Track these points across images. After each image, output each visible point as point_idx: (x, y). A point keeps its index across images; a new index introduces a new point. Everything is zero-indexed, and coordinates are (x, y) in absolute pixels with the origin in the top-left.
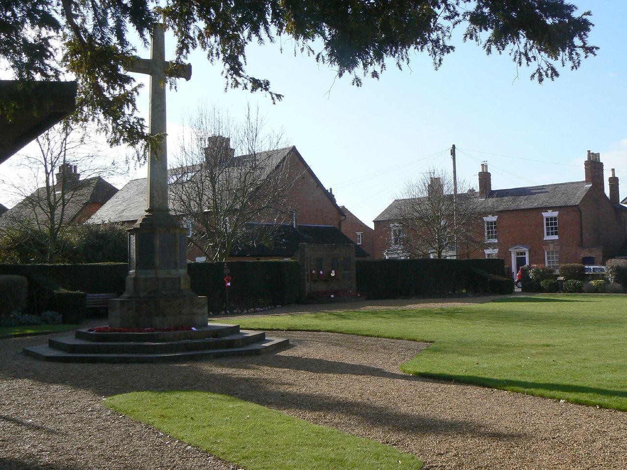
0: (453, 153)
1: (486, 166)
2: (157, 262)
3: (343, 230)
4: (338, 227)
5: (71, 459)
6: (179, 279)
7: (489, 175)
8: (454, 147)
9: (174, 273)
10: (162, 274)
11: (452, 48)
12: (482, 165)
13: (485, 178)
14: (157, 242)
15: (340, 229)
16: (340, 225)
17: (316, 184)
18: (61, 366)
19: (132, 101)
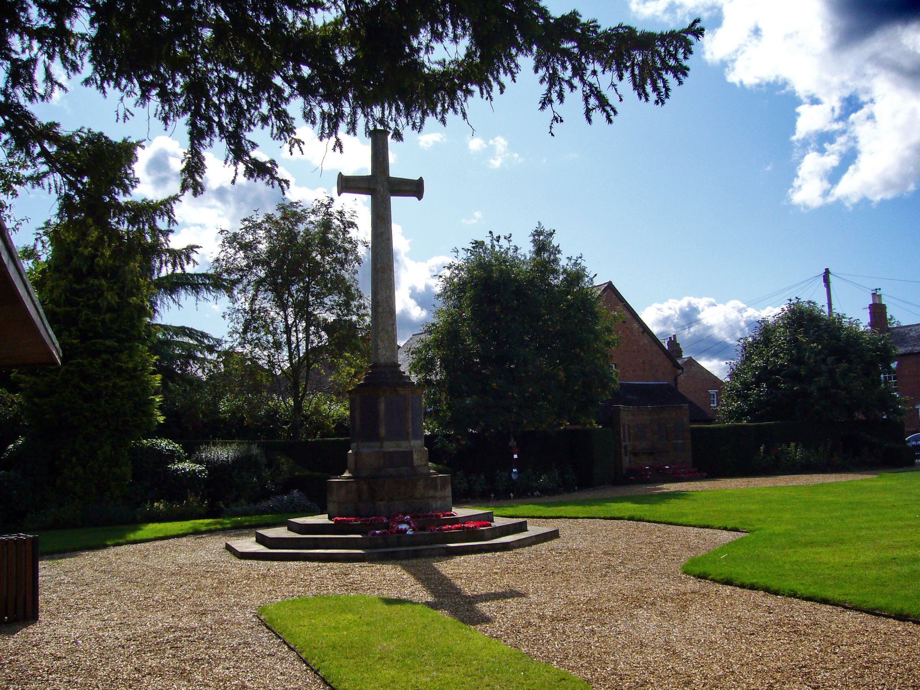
0: (201, 226)
1: (880, 296)
2: (383, 431)
3: (680, 390)
4: (673, 385)
5: (803, 667)
6: (411, 453)
7: (883, 307)
8: (827, 272)
9: (404, 446)
10: (390, 446)
11: (542, 108)
12: (873, 294)
13: (878, 311)
14: (382, 407)
15: (676, 384)
16: (675, 380)
17: (641, 330)
18: (262, 565)
19: (169, 213)
